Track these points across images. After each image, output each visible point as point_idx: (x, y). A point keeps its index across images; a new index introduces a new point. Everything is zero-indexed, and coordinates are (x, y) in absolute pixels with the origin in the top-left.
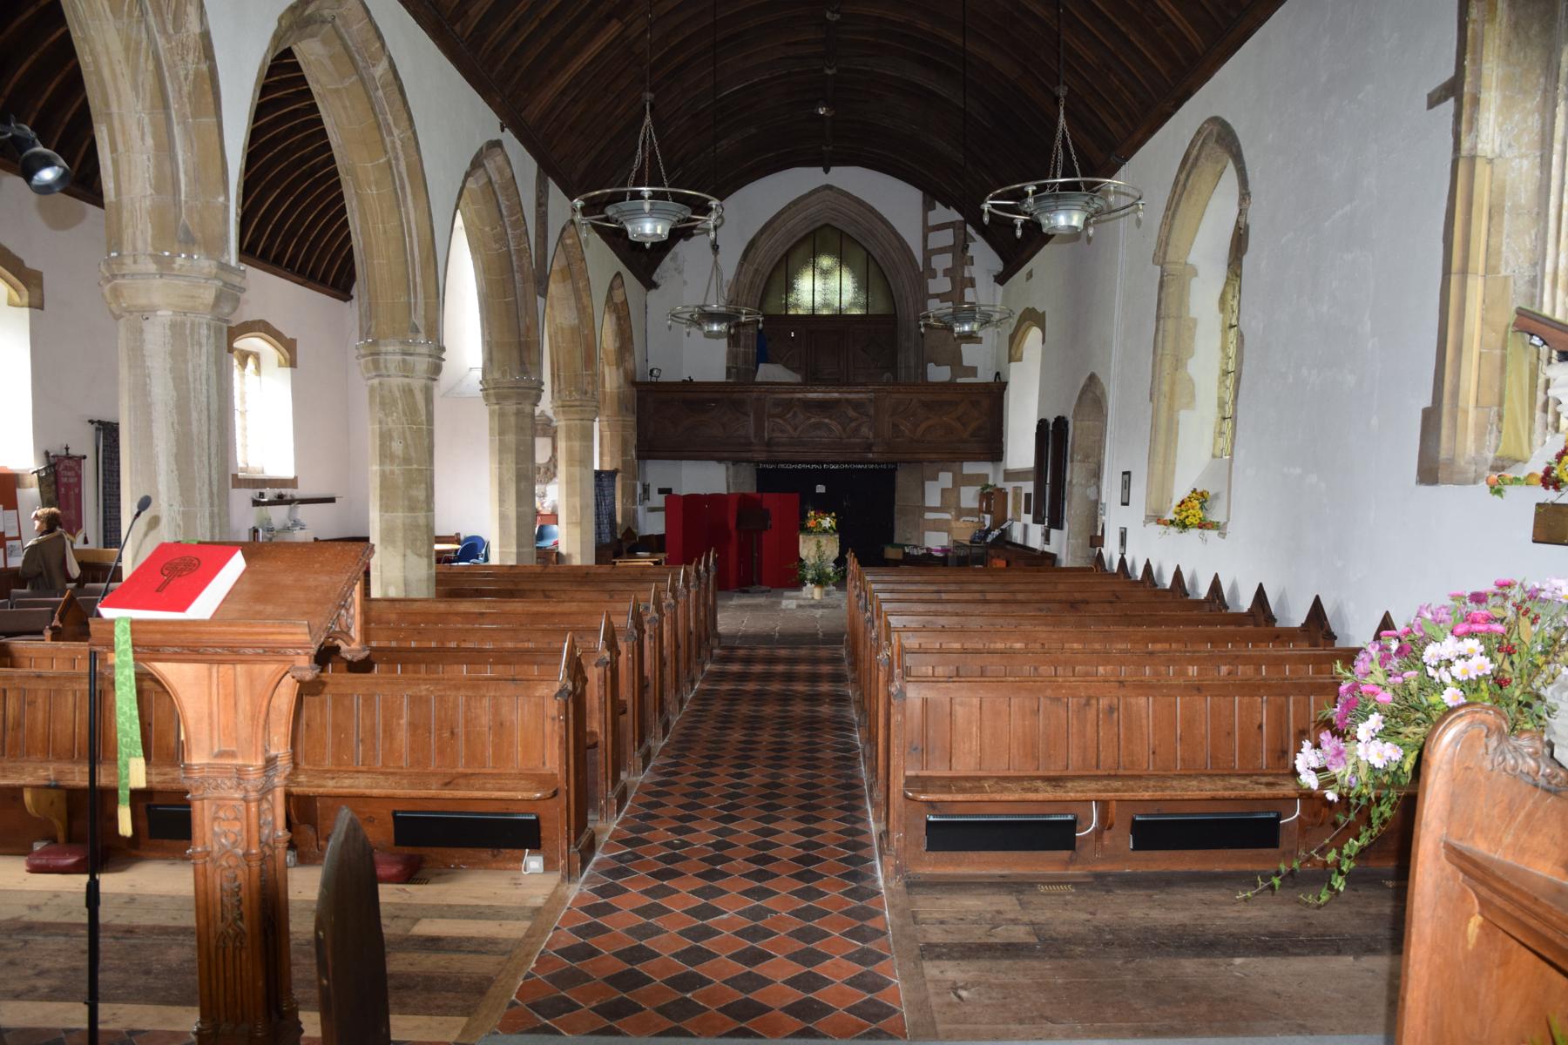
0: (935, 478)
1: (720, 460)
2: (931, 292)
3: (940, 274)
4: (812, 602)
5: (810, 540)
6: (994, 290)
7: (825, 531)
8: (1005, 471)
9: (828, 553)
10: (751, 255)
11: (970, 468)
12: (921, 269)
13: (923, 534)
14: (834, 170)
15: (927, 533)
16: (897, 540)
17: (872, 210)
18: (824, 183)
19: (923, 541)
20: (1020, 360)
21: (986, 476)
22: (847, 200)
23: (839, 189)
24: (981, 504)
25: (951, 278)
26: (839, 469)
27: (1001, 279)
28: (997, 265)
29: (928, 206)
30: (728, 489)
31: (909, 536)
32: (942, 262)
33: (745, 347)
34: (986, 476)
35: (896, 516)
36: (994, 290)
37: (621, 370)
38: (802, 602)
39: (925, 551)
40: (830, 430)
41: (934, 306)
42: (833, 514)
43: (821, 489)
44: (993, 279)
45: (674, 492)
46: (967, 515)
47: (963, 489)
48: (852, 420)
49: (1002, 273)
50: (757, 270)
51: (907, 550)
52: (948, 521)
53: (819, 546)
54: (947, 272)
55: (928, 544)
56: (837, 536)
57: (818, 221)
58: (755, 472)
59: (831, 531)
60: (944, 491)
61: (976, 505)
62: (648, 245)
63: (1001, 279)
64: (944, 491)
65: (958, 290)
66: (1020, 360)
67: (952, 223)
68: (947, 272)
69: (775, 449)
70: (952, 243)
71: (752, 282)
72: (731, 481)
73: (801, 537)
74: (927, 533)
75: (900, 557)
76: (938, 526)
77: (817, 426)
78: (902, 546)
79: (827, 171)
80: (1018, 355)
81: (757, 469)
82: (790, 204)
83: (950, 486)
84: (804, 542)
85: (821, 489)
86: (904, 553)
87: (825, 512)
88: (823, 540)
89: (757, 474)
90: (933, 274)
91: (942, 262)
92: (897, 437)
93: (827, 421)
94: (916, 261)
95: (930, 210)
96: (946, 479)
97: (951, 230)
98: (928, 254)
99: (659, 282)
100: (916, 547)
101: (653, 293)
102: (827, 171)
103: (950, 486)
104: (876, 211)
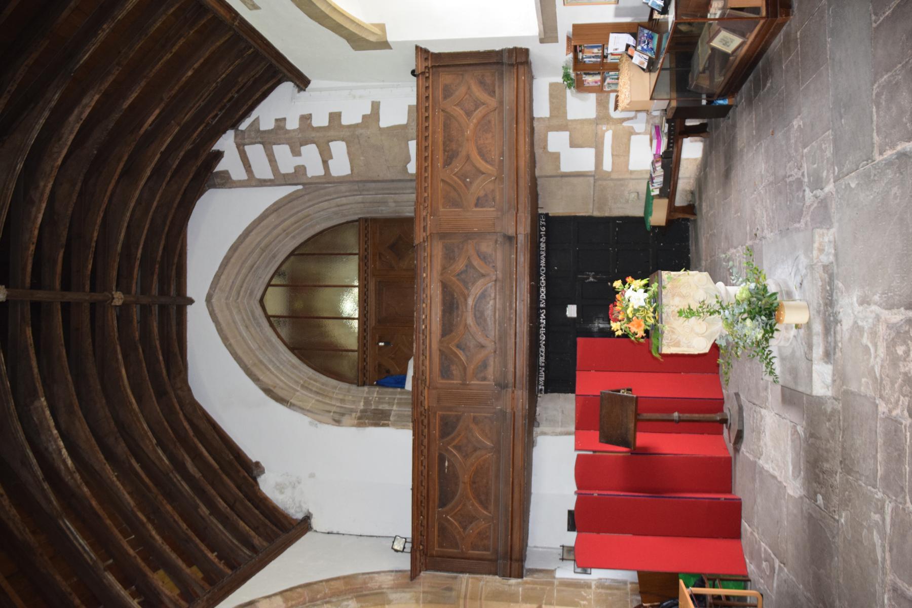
0: (556, 157)
1: (529, 444)
2: (321, 172)
3: (298, 161)
4: (818, 327)
5: (673, 331)
6: (320, 90)
7: (656, 299)
8: (542, 41)
9: (700, 295)
10: (281, 393)
11: (542, 108)
12: (300, 187)
13: (632, 172)
14: (190, 293)
15: (632, 167)
16: (639, 212)
17: (234, 248)
18: (204, 304)
19: (641, 172)
20: (382, 27)
21: (552, 85)
22: (223, 277)
23: (211, 288)
24: (590, 90)
25: (301, 145)
26: (546, 286)
27: (302, 82)
28: (287, 88)
29: (225, 181)
30: (568, 434)
31: (633, 195)
32: (286, 160)
33: (391, 403)
34: (552, 85)
35: (607, 214)
36: (320, 90)
37: (393, 596)
38: (818, 351)
39: (659, 165)
40: (483, 296)
41: (341, 166)
42: (617, 284)
43: (572, 311)
44: (302, 93)
45: (572, 508)
46: (607, 108)
47: (570, 116)
48: (469, 265)
49: (295, 84)
50: (303, 386)
51: (657, 192)
52: (615, 136)
53: (689, 313)
54: (296, 153)
55: (648, 166)
56: (665, 274)
57: (253, 313)
58: (549, 395)
59: (654, 287)
60: (573, 145)
61: (593, 97)
62: (216, 554)
63: (302, 82)
64: (573, 145)
65: (314, 134)
66: (382, 27)
67: (238, 147)
68: (296, 153)
69: (510, 378)
70: (260, 147)
71: (317, 393)
72: (559, 430)
73: (666, 350)
74: (632, 167)
75: (665, 202)
76: (622, 150)
77: (480, 317)
78: (649, 198)
79: (191, 301)
80: (377, 31)
81: (546, 392)
82: (226, 345)
83: (567, 134)
84: (677, 344)
85: (572, 311)
86: (660, 196)
87: (613, 301)
88: (672, 303)
89: (553, 391)
90: (300, 170)
91: (286, 160)
92: (494, 200)
93: (470, 301)
94: (290, 195)
95: (229, 177)
96: (557, 141)
97: (247, 148)
98: (280, 180)
99: (305, 510)
100: (652, 179)
101: (315, 523)
102: (191, 301)
103: (565, 135)
104: (235, 243)
